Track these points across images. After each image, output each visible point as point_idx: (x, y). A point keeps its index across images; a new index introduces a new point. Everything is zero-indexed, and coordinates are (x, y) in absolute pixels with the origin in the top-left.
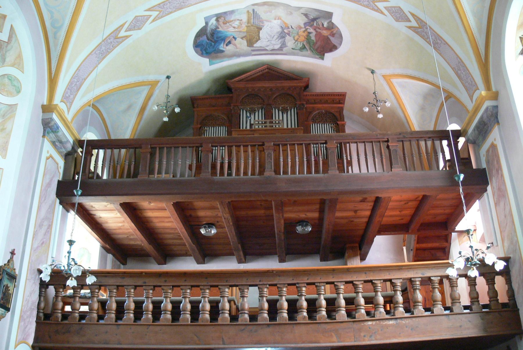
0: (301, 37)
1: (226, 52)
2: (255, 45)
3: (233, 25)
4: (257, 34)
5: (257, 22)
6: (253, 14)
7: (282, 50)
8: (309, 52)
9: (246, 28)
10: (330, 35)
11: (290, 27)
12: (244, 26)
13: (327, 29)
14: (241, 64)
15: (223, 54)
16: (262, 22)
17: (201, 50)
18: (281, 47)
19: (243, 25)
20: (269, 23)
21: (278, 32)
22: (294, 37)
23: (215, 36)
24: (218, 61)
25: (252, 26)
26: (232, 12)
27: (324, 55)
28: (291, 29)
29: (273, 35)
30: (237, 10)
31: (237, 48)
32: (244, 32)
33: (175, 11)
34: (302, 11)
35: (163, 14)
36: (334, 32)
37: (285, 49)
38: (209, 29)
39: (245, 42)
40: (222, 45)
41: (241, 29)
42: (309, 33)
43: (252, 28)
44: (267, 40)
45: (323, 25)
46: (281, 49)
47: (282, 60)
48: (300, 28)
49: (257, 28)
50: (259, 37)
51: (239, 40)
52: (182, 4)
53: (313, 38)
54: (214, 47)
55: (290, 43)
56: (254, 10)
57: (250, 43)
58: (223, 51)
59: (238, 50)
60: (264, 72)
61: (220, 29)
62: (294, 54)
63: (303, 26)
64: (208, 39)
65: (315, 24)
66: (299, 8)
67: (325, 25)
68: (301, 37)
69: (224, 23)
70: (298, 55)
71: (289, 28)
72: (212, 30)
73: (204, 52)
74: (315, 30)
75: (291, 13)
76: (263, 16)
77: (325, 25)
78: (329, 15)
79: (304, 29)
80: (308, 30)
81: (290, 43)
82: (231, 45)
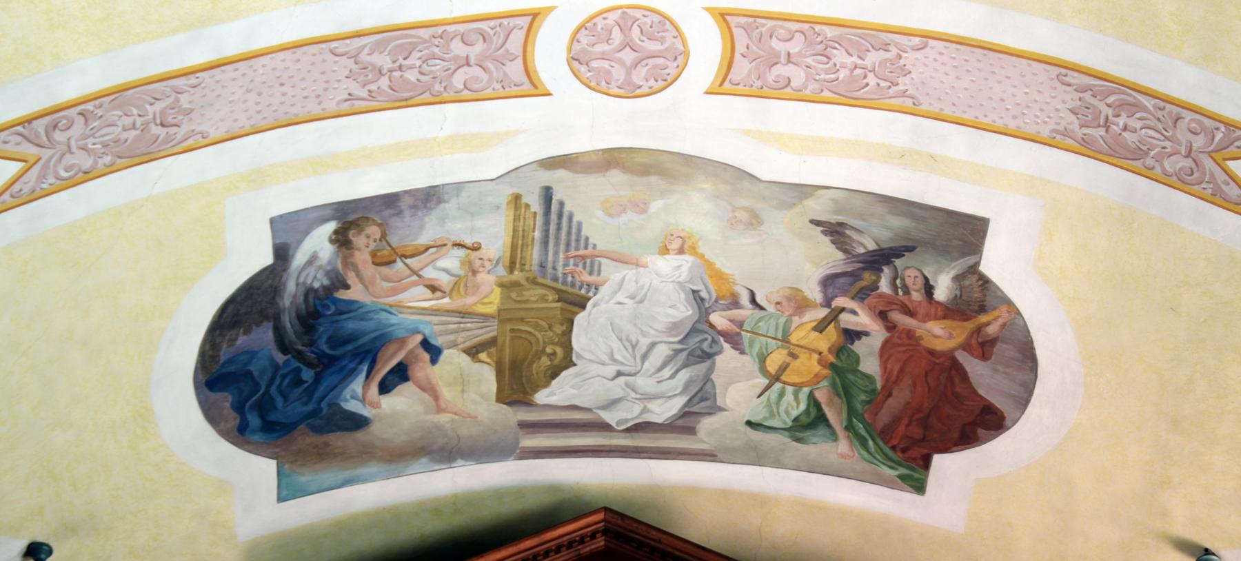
0: (803, 356)
1: (376, 428)
2: (541, 397)
3: (429, 273)
4: (559, 329)
5: (560, 262)
6: (543, 216)
7: (691, 431)
8: (843, 446)
9: (496, 296)
10: (966, 347)
11: (745, 299)
12: (487, 279)
13: (955, 311)
14: (459, 502)
15: (360, 436)
16: (590, 262)
17: (239, 408)
18: (685, 414)
19: (482, 277)
20: (630, 273)
21: (674, 327)
22: (762, 359)
23: (324, 330)
24: (327, 476)
25: (534, 282)
26: (429, 198)
27: (926, 464)
28: (747, 311)
29: (644, 342)
30: (459, 186)
31: (440, 410)
32: (485, 316)
33: (111, 170)
34: (817, 207)
35: (42, 176)
36: (992, 330)
37: (707, 425)
38: (291, 287)
39: (485, 377)
40: (357, 385)
41: (469, 301)
42: (852, 335)
43: (534, 293)
44: (611, 370)
45: (929, 289)
46: (684, 423)
47: (694, 490)
48: (800, 304)
49: (562, 297)
50: (568, 348)
51: (453, 359)
52: (156, 130)
53: (870, 365)
54: (310, 391)
55: (740, 388)
56: (547, 195)
57: (517, 385)
58: (359, 422)
59: (444, 418)
60: (586, 549)
61: (355, 293)
62: (756, 457)
63: (816, 295)
64: (283, 346)
65: (884, 286)
66: (803, 191)
67: (943, 289)
68: (803, 356)
69: (382, 262)
70: (778, 463)
71: (735, 304)
72: (309, 291)
73: (254, 420)
74: (882, 315)
75: (755, 220)
76: (598, 229)
77: (943, 289)
78: (966, 233)
79: (822, 313)
80: (846, 320)
81: (740, 388)
82: (407, 388)
